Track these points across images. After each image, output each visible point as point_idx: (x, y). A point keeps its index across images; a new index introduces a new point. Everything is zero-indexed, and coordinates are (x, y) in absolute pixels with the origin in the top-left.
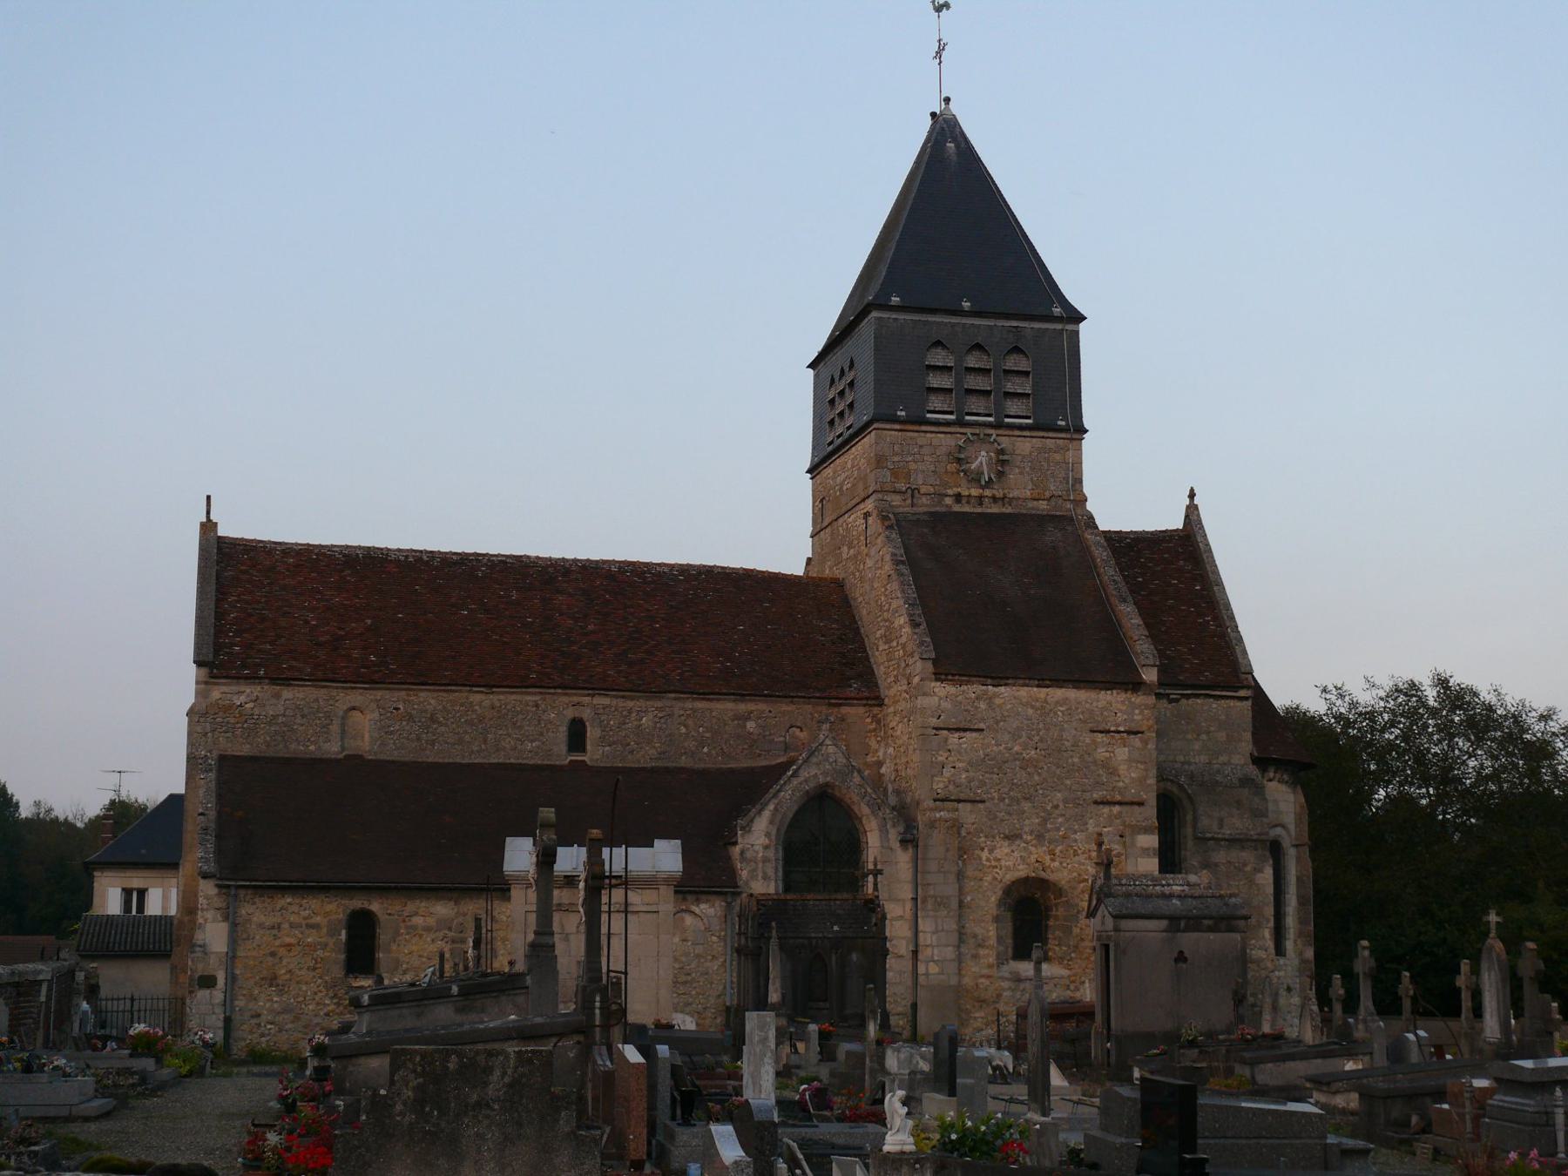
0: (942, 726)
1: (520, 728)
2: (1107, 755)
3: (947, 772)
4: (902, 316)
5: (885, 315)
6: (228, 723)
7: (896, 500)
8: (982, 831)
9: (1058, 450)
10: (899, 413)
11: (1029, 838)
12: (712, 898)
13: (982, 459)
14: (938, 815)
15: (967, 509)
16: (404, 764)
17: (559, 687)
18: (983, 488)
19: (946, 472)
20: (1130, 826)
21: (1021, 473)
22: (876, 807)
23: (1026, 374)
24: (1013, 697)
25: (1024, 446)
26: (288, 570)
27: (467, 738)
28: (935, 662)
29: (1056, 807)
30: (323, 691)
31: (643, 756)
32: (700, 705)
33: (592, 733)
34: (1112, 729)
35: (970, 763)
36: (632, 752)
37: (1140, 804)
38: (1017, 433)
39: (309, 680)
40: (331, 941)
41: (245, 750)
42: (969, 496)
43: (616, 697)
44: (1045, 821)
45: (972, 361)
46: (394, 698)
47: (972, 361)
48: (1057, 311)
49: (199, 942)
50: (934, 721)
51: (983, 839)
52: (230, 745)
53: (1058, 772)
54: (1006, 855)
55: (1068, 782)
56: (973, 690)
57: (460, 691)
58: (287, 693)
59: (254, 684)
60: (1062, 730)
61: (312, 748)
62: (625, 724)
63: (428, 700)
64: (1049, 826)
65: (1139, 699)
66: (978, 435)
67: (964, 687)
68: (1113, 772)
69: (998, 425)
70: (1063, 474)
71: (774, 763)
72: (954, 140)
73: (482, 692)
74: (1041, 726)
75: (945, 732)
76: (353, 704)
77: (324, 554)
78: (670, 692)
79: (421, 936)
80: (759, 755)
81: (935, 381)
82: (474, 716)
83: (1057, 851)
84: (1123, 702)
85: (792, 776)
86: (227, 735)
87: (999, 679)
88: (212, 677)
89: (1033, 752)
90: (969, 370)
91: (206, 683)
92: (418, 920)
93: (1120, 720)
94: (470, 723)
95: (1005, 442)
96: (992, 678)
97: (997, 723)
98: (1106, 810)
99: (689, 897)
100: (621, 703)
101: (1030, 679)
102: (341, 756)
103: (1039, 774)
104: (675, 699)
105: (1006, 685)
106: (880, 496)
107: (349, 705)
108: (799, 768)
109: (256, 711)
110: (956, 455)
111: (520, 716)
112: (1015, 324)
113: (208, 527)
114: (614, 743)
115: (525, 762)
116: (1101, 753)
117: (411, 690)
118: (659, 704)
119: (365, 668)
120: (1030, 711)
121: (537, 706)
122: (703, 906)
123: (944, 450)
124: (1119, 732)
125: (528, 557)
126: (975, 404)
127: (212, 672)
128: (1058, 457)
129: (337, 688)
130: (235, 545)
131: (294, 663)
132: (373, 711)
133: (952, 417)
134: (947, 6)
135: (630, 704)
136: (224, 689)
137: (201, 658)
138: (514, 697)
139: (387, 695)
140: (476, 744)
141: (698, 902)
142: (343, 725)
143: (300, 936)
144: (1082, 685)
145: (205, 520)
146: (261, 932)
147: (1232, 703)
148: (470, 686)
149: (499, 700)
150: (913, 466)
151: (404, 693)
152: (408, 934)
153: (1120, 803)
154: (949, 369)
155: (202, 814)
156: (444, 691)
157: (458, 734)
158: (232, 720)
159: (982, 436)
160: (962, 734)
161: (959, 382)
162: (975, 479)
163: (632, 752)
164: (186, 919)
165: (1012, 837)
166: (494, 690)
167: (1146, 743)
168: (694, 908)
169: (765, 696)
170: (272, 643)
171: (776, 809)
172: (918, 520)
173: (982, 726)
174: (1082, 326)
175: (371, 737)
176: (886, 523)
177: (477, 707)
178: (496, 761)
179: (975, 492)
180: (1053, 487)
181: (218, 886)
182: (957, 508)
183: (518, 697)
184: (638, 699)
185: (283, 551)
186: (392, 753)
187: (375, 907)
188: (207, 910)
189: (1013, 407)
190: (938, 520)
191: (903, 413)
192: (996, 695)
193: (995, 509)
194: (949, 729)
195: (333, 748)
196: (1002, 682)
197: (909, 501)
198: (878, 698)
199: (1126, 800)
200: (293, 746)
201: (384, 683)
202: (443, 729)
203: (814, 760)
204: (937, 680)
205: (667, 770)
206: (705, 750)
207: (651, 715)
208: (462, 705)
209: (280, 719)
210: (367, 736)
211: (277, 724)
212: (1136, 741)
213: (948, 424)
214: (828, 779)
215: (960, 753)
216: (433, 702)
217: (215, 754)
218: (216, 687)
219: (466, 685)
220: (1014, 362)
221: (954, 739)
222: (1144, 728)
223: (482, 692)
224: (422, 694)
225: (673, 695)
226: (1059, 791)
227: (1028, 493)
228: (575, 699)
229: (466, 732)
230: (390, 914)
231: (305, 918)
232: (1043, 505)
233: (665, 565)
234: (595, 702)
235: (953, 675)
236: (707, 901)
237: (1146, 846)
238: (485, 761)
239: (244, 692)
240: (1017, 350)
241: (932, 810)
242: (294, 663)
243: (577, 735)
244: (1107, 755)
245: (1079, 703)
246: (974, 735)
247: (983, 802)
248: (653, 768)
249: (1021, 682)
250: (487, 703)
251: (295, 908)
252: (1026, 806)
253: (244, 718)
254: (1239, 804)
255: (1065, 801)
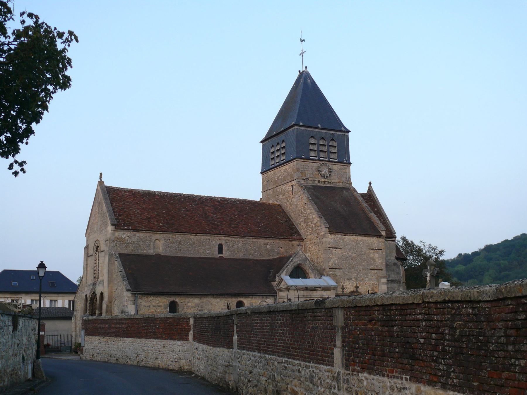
0: (331, 247)
1: (205, 246)
2: (373, 256)
3: (332, 260)
4: (303, 128)
5: (299, 128)
6: (120, 243)
7: (302, 181)
8: (342, 278)
9: (344, 169)
10: (303, 156)
11: (354, 279)
12: (271, 297)
13: (325, 170)
14: (331, 273)
15: (321, 185)
16: (173, 257)
17: (216, 234)
18: (325, 179)
19: (315, 174)
20: (379, 276)
21: (335, 175)
22: (313, 271)
23: (335, 147)
24: (349, 239)
25: (335, 167)
26: (127, 197)
27: (190, 249)
28: (329, 228)
29: (360, 271)
30: (149, 234)
31: (239, 255)
32: (254, 240)
33: (225, 248)
34: (374, 248)
35: (338, 258)
36: (236, 254)
37: (382, 270)
38: (334, 163)
39: (144, 230)
40: (165, 311)
41: (125, 252)
42: (322, 181)
43: (231, 237)
44: (358, 274)
45: (322, 142)
46: (169, 236)
47: (322, 142)
48: (343, 129)
49: (127, 311)
50: (329, 246)
51: (342, 280)
52: (121, 250)
53: (361, 260)
54: (348, 284)
55: (363, 263)
56: (339, 236)
57: (188, 235)
58: (138, 234)
59: (128, 231)
60: (362, 248)
61: (145, 251)
62: (234, 245)
63: (179, 237)
64: (359, 276)
65: (381, 240)
66: (324, 164)
67: (336, 236)
68: (375, 261)
69: (329, 161)
70: (345, 176)
71: (275, 258)
72: (310, 79)
73: (194, 235)
74: (356, 247)
75: (332, 249)
76: (157, 238)
77: (136, 192)
78: (247, 236)
79: (190, 309)
80: (271, 255)
81: (312, 147)
82: (192, 243)
83: (361, 283)
84: (377, 241)
85: (291, 261)
86: (120, 247)
87: (346, 234)
88: (116, 229)
89: (354, 255)
90: (321, 145)
91: (114, 231)
92: (189, 304)
93: (375, 246)
94: (191, 244)
95: (331, 166)
96: (344, 233)
97: (345, 246)
98: (373, 271)
99: (264, 297)
100: (233, 239)
101: (354, 234)
102: (154, 254)
103: (356, 261)
104: (248, 238)
105: (347, 235)
106: (298, 180)
107: (156, 239)
108: (292, 259)
109: (129, 240)
110: (318, 169)
111: (205, 243)
112: (332, 132)
113: (101, 183)
114: (231, 251)
115: (206, 257)
116: (371, 255)
117: (174, 234)
118: (243, 240)
119: (160, 227)
120: (353, 243)
121: (209, 240)
122: (268, 300)
123: (314, 167)
124: (376, 249)
125: (194, 195)
126: (322, 155)
127: (116, 227)
128: (344, 171)
129: (152, 233)
130: (110, 188)
131: (139, 225)
132: (163, 240)
133: (317, 158)
134: (304, 40)
135: (235, 240)
136: (119, 233)
137: (113, 223)
138: (203, 237)
139: (167, 235)
140: (193, 251)
141: (267, 298)
142: (154, 244)
143: (156, 309)
144: (367, 236)
145: (99, 180)
146: (144, 308)
147: (391, 242)
148: (191, 233)
149: (199, 238)
150: (306, 172)
151: (172, 235)
152: (187, 308)
153: (376, 270)
154: (315, 144)
155: (120, 271)
156: (183, 235)
157: (187, 248)
158: (122, 243)
159: (325, 164)
160: (336, 249)
161: (318, 148)
162: (323, 176)
163: (236, 254)
164: (109, 305)
165: (349, 279)
166: (198, 234)
167: (382, 252)
168: (266, 300)
169: (273, 238)
170: (130, 219)
171: (287, 271)
172: (309, 187)
173: (341, 247)
174: (349, 133)
175: (162, 248)
176: (303, 188)
177: (192, 240)
178: (198, 256)
179: (323, 180)
180: (343, 180)
181: (132, 294)
182: (319, 184)
183: (204, 237)
184: (237, 238)
185: (124, 191)
186: (168, 253)
187: (177, 300)
188: (128, 301)
189: (332, 156)
190: (315, 188)
191: (304, 156)
192: (345, 238)
193: (329, 185)
194: (332, 248)
195: (151, 252)
196: (346, 234)
197: (306, 182)
198: (302, 239)
199: (378, 269)
200: (139, 251)
201: (166, 232)
202: (183, 246)
203: (297, 256)
204: (329, 233)
205: (246, 259)
206: (256, 254)
207: (241, 243)
208: (188, 239)
209: (136, 242)
210: (161, 248)
211: (135, 244)
212: (380, 252)
213: (316, 160)
214: (301, 262)
215: (335, 255)
216: (180, 238)
217: (117, 253)
218: (117, 232)
219: (190, 233)
220: (332, 143)
221: (334, 250)
222: (382, 248)
223: (194, 235)
224: (177, 235)
225: (247, 237)
226: (361, 266)
227: (337, 181)
228: (220, 238)
229: (189, 247)
230: (181, 302)
231: (157, 304)
232: (341, 184)
233: (233, 199)
234: (226, 239)
235: (334, 232)
236: (269, 298)
237: (383, 282)
238: (195, 256)
239: (125, 234)
240: (333, 140)
241: (329, 271)
242: (139, 225)
243: (220, 248)
244: (373, 256)
245: (366, 241)
246: (339, 250)
247: (342, 269)
248: (242, 259)
249: (351, 234)
250: (195, 239)
251: (154, 300)
252: (353, 270)
253: (125, 242)
254: (393, 270)
255: (363, 269)
